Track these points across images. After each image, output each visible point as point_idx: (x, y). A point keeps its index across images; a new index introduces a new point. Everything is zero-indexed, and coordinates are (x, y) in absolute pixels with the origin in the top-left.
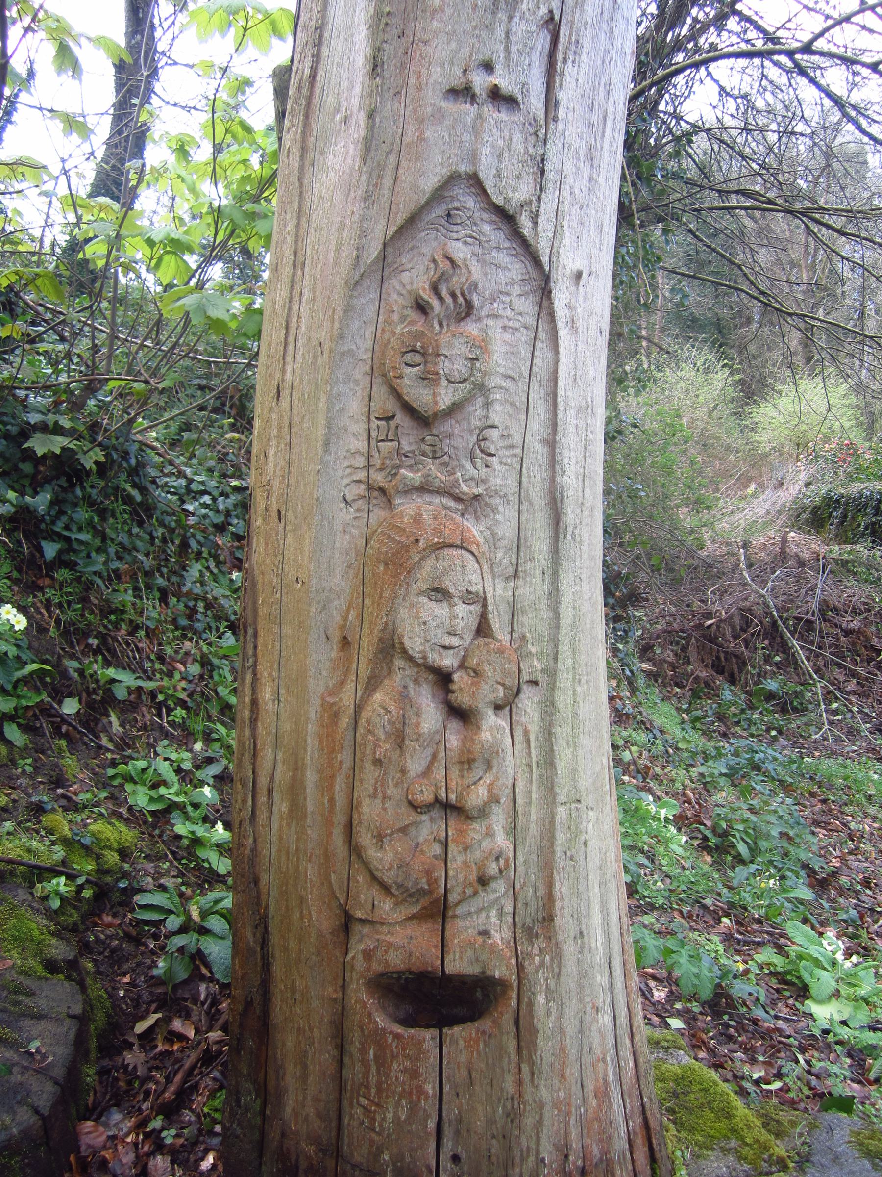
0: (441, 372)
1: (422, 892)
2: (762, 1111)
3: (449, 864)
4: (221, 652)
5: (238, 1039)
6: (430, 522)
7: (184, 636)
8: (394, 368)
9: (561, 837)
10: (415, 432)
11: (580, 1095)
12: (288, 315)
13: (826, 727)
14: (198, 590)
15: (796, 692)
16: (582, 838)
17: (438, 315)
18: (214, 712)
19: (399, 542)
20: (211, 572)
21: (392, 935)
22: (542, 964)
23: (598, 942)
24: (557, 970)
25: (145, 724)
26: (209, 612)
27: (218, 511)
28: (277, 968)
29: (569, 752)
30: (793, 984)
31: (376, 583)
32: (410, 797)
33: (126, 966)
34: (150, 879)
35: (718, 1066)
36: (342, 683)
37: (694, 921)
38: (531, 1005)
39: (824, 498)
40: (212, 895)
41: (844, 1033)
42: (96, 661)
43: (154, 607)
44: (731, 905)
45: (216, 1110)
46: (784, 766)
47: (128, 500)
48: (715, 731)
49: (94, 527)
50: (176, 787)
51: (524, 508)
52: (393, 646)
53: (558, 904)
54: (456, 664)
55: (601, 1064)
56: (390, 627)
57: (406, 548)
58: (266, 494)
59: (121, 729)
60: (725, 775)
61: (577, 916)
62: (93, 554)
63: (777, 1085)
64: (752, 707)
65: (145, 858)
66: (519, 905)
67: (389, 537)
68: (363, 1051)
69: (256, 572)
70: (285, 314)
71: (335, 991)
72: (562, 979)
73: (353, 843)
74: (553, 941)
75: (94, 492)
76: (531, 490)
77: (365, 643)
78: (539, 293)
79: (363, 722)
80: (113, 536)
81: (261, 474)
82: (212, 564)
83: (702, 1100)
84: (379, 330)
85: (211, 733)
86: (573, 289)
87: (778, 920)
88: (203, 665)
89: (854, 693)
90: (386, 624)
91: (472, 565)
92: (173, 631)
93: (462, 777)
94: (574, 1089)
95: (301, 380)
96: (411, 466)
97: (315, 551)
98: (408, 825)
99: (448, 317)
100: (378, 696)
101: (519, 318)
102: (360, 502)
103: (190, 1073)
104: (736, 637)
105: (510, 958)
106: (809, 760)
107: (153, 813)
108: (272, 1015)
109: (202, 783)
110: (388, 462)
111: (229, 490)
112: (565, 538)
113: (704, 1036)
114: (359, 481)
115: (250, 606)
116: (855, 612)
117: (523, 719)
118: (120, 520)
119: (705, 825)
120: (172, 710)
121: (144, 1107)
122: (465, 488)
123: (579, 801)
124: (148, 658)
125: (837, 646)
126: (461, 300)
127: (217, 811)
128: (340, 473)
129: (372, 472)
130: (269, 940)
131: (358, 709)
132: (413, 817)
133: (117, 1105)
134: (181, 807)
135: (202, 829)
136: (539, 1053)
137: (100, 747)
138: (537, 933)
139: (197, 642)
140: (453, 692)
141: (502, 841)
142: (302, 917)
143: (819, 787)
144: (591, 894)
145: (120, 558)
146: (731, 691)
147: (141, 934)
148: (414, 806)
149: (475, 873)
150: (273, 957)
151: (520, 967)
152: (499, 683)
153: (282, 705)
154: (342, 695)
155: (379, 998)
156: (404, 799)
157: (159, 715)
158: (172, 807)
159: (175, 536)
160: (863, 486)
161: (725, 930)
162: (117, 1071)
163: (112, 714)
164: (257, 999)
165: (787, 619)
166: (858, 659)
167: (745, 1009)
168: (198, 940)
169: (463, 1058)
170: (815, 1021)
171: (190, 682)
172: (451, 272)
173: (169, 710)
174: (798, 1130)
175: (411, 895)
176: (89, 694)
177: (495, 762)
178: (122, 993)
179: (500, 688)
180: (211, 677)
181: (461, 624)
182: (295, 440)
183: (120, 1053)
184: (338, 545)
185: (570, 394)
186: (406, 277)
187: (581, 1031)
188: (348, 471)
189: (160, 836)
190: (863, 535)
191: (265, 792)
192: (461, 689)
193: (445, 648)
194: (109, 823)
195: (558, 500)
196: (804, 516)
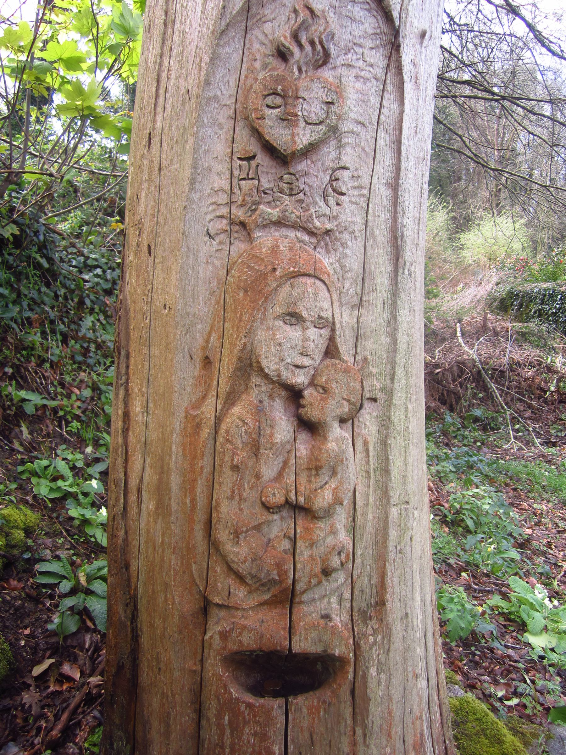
0: (300, 113)
1: (273, 582)
2: (510, 725)
3: (297, 558)
4: (108, 381)
5: (112, 696)
6: (286, 252)
7: (80, 368)
8: (256, 110)
9: (393, 533)
10: (274, 171)
11: (402, 749)
12: (159, 70)
13: (513, 440)
14: (90, 335)
15: (493, 417)
16: (409, 534)
17: (298, 62)
18: (101, 424)
19: (258, 271)
20: (101, 323)
21: (246, 619)
22: (375, 642)
23: (418, 621)
24: (387, 647)
25: (49, 433)
26: (99, 352)
27: (106, 280)
28: (145, 640)
29: (401, 460)
30: (516, 621)
31: (236, 308)
32: (263, 499)
33: (27, 621)
34: (48, 552)
35: (472, 687)
36: (204, 398)
37: (444, 575)
38: (365, 677)
39: (509, 293)
40: (97, 564)
41: (554, 658)
42: (11, 385)
43: (58, 347)
44: (468, 563)
45: (95, 745)
46: (488, 466)
47: (38, 266)
48: (441, 442)
49: (12, 286)
50: (71, 480)
51: (369, 244)
52: (251, 365)
53: (389, 591)
54: (306, 382)
55: (419, 722)
56: (249, 348)
57: (264, 276)
58: (137, 233)
59: (29, 436)
60: (454, 472)
61: (405, 600)
62: (11, 305)
63: (515, 701)
64: (464, 427)
65: (45, 534)
66: (356, 592)
67: (249, 266)
68: (219, 716)
69: (129, 302)
70: (156, 70)
71: (195, 664)
72: (391, 654)
73: (212, 538)
74: (385, 622)
75: (11, 259)
76: (376, 228)
77: (225, 361)
78: (389, 47)
79: (222, 432)
80: (26, 292)
81: (134, 215)
82: (102, 317)
83: (478, 728)
84: (243, 77)
85: (99, 439)
86: (418, 47)
87: (499, 574)
88: (93, 390)
89: (529, 418)
90: (245, 345)
91: (323, 293)
92: (71, 365)
93: (310, 481)
94: (397, 745)
95: (170, 127)
96: (269, 203)
97: (181, 280)
98: (261, 523)
99: (307, 64)
100: (236, 410)
101: (370, 69)
102: (223, 236)
103: (74, 712)
104: (454, 381)
105: (348, 639)
106: (503, 462)
107: (52, 500)
108: (140, 679)
109: (90, 477)
110: (248, 199)
111: (115, 265)
112: (403, 273)
113: (460, 664)
114: (222, 217)
115: (123, 331)
116: (532, 365)
117: (363, 431)
118: (32, 281)
119: (443, 506)
120: (70, 423)
121: (36, 741)
122: (317, 224)
123: (407, 502)
124: (52, 383)
125: (519, 388)
126: (319, 47)
127: (103, 498)
128: (204, 210)
129: (233, 208)
130: (137, 617)
131: (218, 421)
132: (267, 516)
133: (14, 740)
134: (74, 496)
135: (90, 512)
136: (370, 718)
137: (13, 450)
138: (371, 616)
139: (89, 373)
140: (303, 407)
141: (343, 537)
142: (166, 600)
143: (511, 480)
144: (414, 581)
145: (31, 310)
146: (451, 416)
147: (40, 594)
148: (267, 507)
149: (319, 566)
150: (141, 631)
151: (357, 646)
152: (344, 399)
153: (150, 417)
154: (203, 409)
155: (233, 671)
156: (258, 501)
157: (60, 427)
158: (67, 495)
159: (74, 295)
160: (534, 285)
161: (465, 582)
162: (16, 709)
163: (23, 425)
164: (128, 664)
165: (488, 370)
166: (533, 396)
167: (483, 641)
168: (85, 599)
169: (306, 723)
170: (533, 649)
171: (84, 402)
172: (310, 21)
173: (68, 423)
174: (539, 742)
175: (263, 585)
176: (5, 410)
177: (339, 469)
178: (23, 643)
179: (346, 404)
180: (100, 399)
181: (313, 346)
182: (164, 182)
183: (19, 694)
184: (201, 275)
185: (411, 143)
186: (268, 27)
187: (404, 696)
188: (212, 207)
189: (57, 518)
190: (533, 317)
191: (135, 491)
192: (311, 404)
193: (297, 367)
194: (17, 508)
195: (399, 238)
196: (495, 304)
